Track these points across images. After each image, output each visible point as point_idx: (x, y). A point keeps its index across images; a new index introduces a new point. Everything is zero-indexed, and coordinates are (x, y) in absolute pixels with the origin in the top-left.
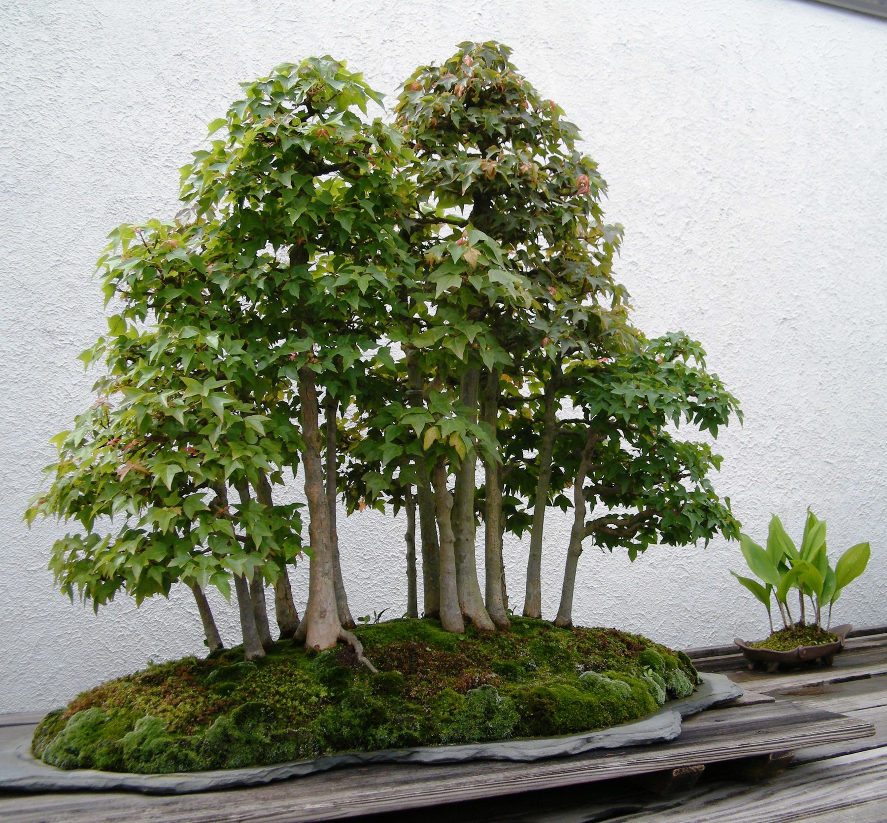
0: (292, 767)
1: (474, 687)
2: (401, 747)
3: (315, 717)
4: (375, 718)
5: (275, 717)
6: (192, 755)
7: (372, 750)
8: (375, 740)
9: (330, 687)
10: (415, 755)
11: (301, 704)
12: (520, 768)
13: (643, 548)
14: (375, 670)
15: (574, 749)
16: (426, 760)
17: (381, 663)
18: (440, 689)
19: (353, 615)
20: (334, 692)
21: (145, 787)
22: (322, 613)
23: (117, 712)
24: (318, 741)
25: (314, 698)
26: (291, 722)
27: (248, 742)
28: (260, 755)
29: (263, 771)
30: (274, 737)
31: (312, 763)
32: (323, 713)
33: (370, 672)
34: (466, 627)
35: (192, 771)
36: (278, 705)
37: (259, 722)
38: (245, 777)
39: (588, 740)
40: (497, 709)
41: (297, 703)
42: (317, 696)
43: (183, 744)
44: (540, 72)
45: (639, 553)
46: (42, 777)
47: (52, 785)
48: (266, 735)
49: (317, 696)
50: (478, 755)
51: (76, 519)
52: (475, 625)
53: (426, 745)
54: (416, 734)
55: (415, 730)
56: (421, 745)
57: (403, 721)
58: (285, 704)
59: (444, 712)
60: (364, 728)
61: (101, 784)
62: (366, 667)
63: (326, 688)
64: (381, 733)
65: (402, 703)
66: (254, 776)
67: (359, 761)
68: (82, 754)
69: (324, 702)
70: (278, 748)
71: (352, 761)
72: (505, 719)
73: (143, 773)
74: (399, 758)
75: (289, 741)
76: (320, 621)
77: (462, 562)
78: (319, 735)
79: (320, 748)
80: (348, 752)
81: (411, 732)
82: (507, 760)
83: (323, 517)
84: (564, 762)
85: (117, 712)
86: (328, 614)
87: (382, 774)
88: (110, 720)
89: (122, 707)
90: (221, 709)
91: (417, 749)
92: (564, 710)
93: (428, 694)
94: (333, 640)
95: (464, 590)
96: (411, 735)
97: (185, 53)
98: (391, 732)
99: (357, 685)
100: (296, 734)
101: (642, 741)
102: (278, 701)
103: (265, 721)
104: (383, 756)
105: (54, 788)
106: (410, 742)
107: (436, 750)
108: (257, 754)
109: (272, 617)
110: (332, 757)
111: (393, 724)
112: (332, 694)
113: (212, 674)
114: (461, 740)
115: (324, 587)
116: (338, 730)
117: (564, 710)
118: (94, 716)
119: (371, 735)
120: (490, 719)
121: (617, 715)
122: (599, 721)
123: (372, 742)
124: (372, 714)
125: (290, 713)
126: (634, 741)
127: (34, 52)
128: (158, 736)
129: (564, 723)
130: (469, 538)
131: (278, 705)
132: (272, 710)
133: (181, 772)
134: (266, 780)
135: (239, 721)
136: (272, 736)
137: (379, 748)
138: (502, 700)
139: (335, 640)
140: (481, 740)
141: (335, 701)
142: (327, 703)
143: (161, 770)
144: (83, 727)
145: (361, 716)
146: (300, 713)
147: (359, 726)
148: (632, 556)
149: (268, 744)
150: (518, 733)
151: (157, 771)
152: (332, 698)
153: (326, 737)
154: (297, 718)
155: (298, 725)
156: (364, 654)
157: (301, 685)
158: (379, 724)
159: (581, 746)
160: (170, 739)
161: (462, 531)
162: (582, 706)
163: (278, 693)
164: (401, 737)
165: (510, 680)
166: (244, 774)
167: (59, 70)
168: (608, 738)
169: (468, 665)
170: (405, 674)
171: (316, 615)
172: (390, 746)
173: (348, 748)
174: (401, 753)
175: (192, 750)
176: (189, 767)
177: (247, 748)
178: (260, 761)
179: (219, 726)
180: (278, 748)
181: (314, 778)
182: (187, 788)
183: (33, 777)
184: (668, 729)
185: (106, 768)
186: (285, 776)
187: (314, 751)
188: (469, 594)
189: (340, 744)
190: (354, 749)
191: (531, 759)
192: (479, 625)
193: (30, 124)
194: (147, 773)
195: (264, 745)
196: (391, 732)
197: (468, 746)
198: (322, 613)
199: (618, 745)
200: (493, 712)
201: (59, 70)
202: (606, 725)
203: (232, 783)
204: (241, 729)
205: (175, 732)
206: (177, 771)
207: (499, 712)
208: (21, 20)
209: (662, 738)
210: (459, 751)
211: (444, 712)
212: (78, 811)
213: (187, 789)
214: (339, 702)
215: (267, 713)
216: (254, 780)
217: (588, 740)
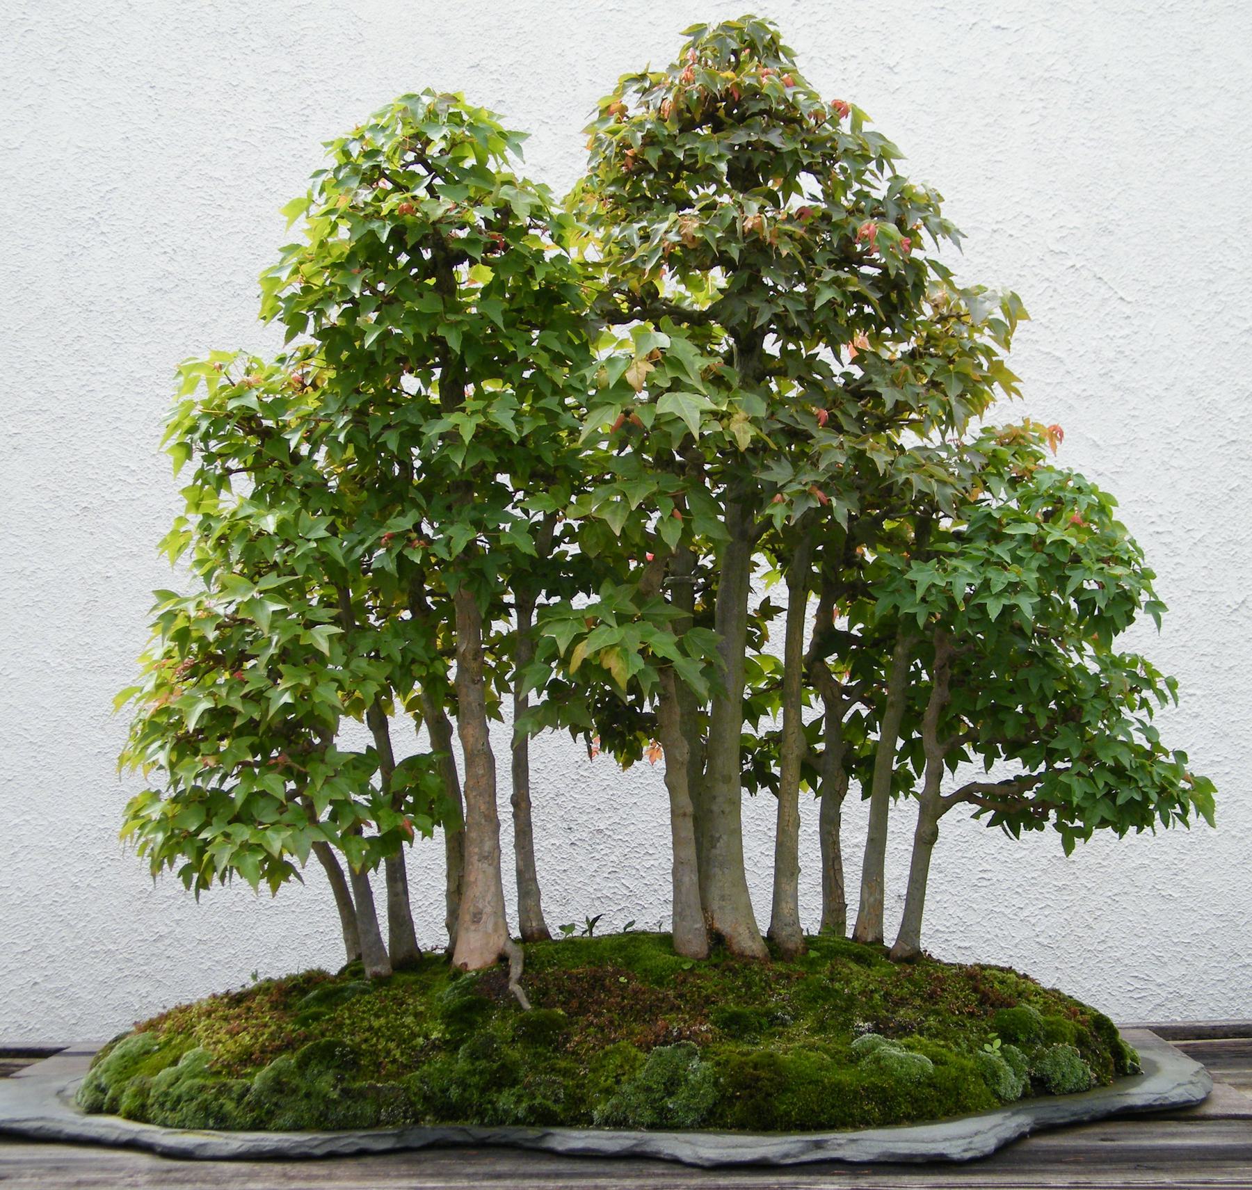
0: (361, 1137)
1: (665, 1043)
2: (533, 1125)
3: (417, 1068)
4: (504, 1077)
5: (355, 1063)
6: (229, 1106)
7: (491, 1124)
8: (495, 1110)
9: (448, 1025)
10: (548, 1138)
11: (398, 1046)
12: (691, 1176)
13: (1085, 834)
14: (527, 1006)
15: (786, 1156)
16: (560, 1148)
17: (540, 998)
18: (613, 1041)
19: (547, 921)
20: (451, 1034)
21: (160, 1145)
22: (475, 915)
23: (170, 1040)
24: (413, 1104)
25: (420, 1040)
26: (379, 1072)
27: (308, 1095)
28: (321, 1116)
29: (315, 1139)
30: (346, 1093)
31: (393, 1135)
32: (429, 1063)
33: (519, 1008)
34: (710, 949)
35: (227, 1129)
36: (364, 1046)
37: (328, 1068)
38: (286, 1144)
39: (818, 1145)
40: (686, 1080)
41: (392, 1045)
42: (426, 1037)
43: (223, 1090)
44: (827, 69)
45: (1078, 841)
46: (52, 1120)
47: (60, 1132)
48: (335, 1087)
49: (426, 1037)
50: (638, 1149)
51: (369, 748)
52: (729, 948)
53: (571, 1126)
54: (557, 1108)
55: (556, 1101)
56: (562, 1124)
57: (540, 1084)
58: (375, 1045)
59: (607, 1077)
60: (484, 1090)
61: (113, 1136)
62: (516, 1000)
63: (442, 1027)
64: (505, 1100)
65: (550, 1058)
66: (300, 1144)
67: (470, 1140)
68: (110, 1092)
69: (435, 1046)
70: (348, 1108)
71: (458, 1138)
72: (770, 1095)
73: (166, 1126)
74: (527, 1140)
75: (365, 1098)
76: (473, 928)
77: (714, 847)
78: (415, 1094)
79: (414, 1114)
80: (459, 1124)
81: (549, 1103)
82: (676, 1161)
83: (481, 772)
84: (942, 1173)
85: (170, 1040)
86: (484, 917)
87: (487, 1161)
88: (159, 1049)
89: (179, 1033)
90: (289, 1046)
91: (552, 1130)
92: (793, 1092)
93: (593, 1048)
94: (490, 957)
95: (714, 892)
96: (548, 1109)
97: (484, 62)
98: (519, 1101)
99: (498, 1026)
100: (379, 1090)
101: (906, 1156)
102: (366, 1041)
103: (338, 1067)
104: (505, 1136)
105: (62, 1136)
106: (547, 1119)
107: (575, 1133)
108: (317, 1114)
109: (512, 909)
110: (431, 1128)
111: (525, 1088)
112: (448, 1036)
113: (312, 994)
114: (617, 1123)
115: (481, 876)
116: (444, 1091)
117: (793, 1092)
118: (140, 1043)
119: (490, 1102)
120: (670, 1094)
121: (891, 1109)
122: (852, 1115)
123: (491, 1112)
124: (497, 1071)
125: (381, 1059)
126: (893, 1155)
127: (271, 89)
128: (195, 1076)
129: (788, 1114)
130: (727, 810)
131: (364, 1046)
132: (352, 1052)
133: (212, 1129)
134: (318, 1152)
135: (303, 1064)
136: (343, 1090)
137: (501, 1123)
138: (698, 1069)
139: (494, 957)
140: (653, 1127)
141: (451, 1046)
142: (439, 1048)
143: (188, 1123)
144: (123, 1056)
145: (481, 1073)
146: (394, 1061)
147: (476, 1086)
148: (1068, 847)
149: (334, 1101)
150: (711, 1121)
151: (181, 1125)
152: (447, 1042)
153: (426, 1099)
154: (389, 1066)
155: (390, 1076)
156: (519, 982)
157: (409, 1020)
158: (504, 1086)
159: (803, 1153)
160: (210, 1082)
161: (714, 798)
162: (824, 1088)
163: (370, 1028)
164: (531, 1109)
165: (733, 1036)
166: (287, 1140)
167: (306, 112)
168: (853, 1146)
169: (674, 1008)
170: (570, 1015)
171: (468, 917)
172: (517, 1121)
173: (457, 1119)
174: (532, 1133)
175: (232, 1099)
176: (223, 1123)
177: (303, 1105)
178: (320, 1124)
179: (273, 1069)
180: (348, 1108)
181: (393, 1158)
182: (209, 1152)
183: (42, 1119)
184: (961, 1142)
185: (130, 1116)
186: (348, 1150)
187: (406, 1118)
188: (723, 898)
189: (449, 1112)
190: (455, 1120)
191: (706, 1164)
192: (735, 947)
193: (267, 195)
194: (171, 1127)
195: (329, 1102)
196: (519, 1101)
197: (626, 1134)
198: (475, 915)
199: (865, 1158)
200: (679, 1085)
201: (306, 112)
202: (866, 1122)
203: (269, 1152)
204: (303, 1075)
205: (219, 1073)
206: (206, 1127)
207: (687, 1085)
208: (253, 46)
209: (942, 1155)
210: (612, 1138)
211: (607, 1077)
212: (58, 1168)
213: (209, 1153)
214: (456, 1049)
215: (343, 1055)
216: (298, 1151)
217: (818, 1145)
